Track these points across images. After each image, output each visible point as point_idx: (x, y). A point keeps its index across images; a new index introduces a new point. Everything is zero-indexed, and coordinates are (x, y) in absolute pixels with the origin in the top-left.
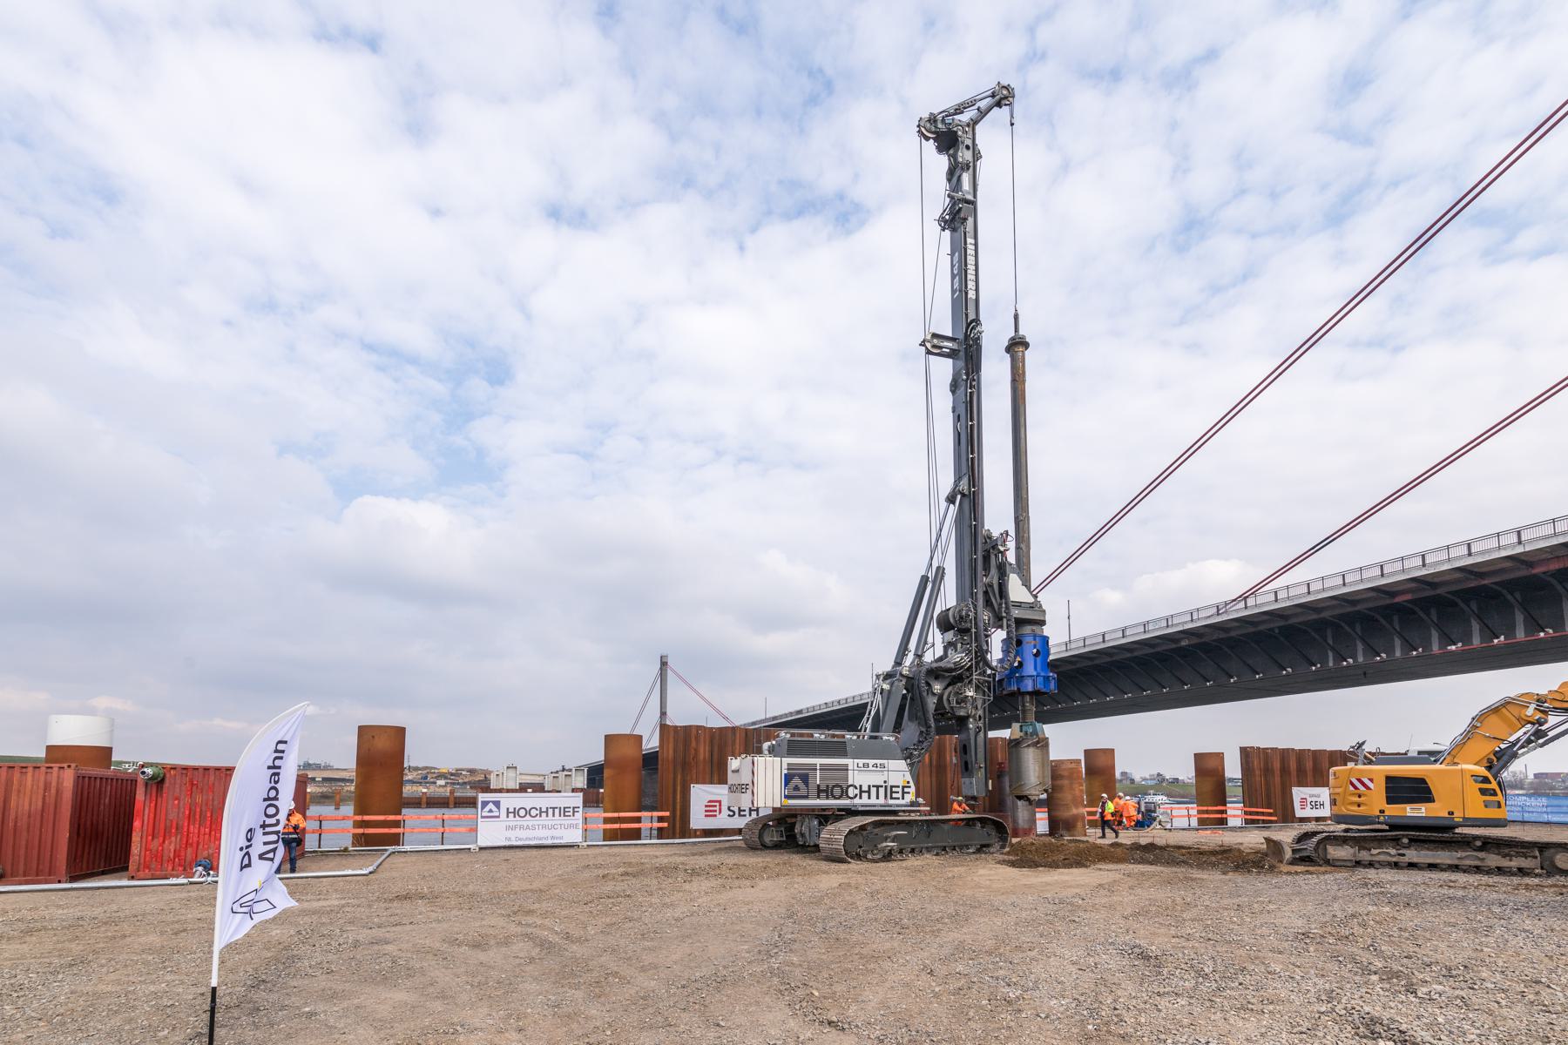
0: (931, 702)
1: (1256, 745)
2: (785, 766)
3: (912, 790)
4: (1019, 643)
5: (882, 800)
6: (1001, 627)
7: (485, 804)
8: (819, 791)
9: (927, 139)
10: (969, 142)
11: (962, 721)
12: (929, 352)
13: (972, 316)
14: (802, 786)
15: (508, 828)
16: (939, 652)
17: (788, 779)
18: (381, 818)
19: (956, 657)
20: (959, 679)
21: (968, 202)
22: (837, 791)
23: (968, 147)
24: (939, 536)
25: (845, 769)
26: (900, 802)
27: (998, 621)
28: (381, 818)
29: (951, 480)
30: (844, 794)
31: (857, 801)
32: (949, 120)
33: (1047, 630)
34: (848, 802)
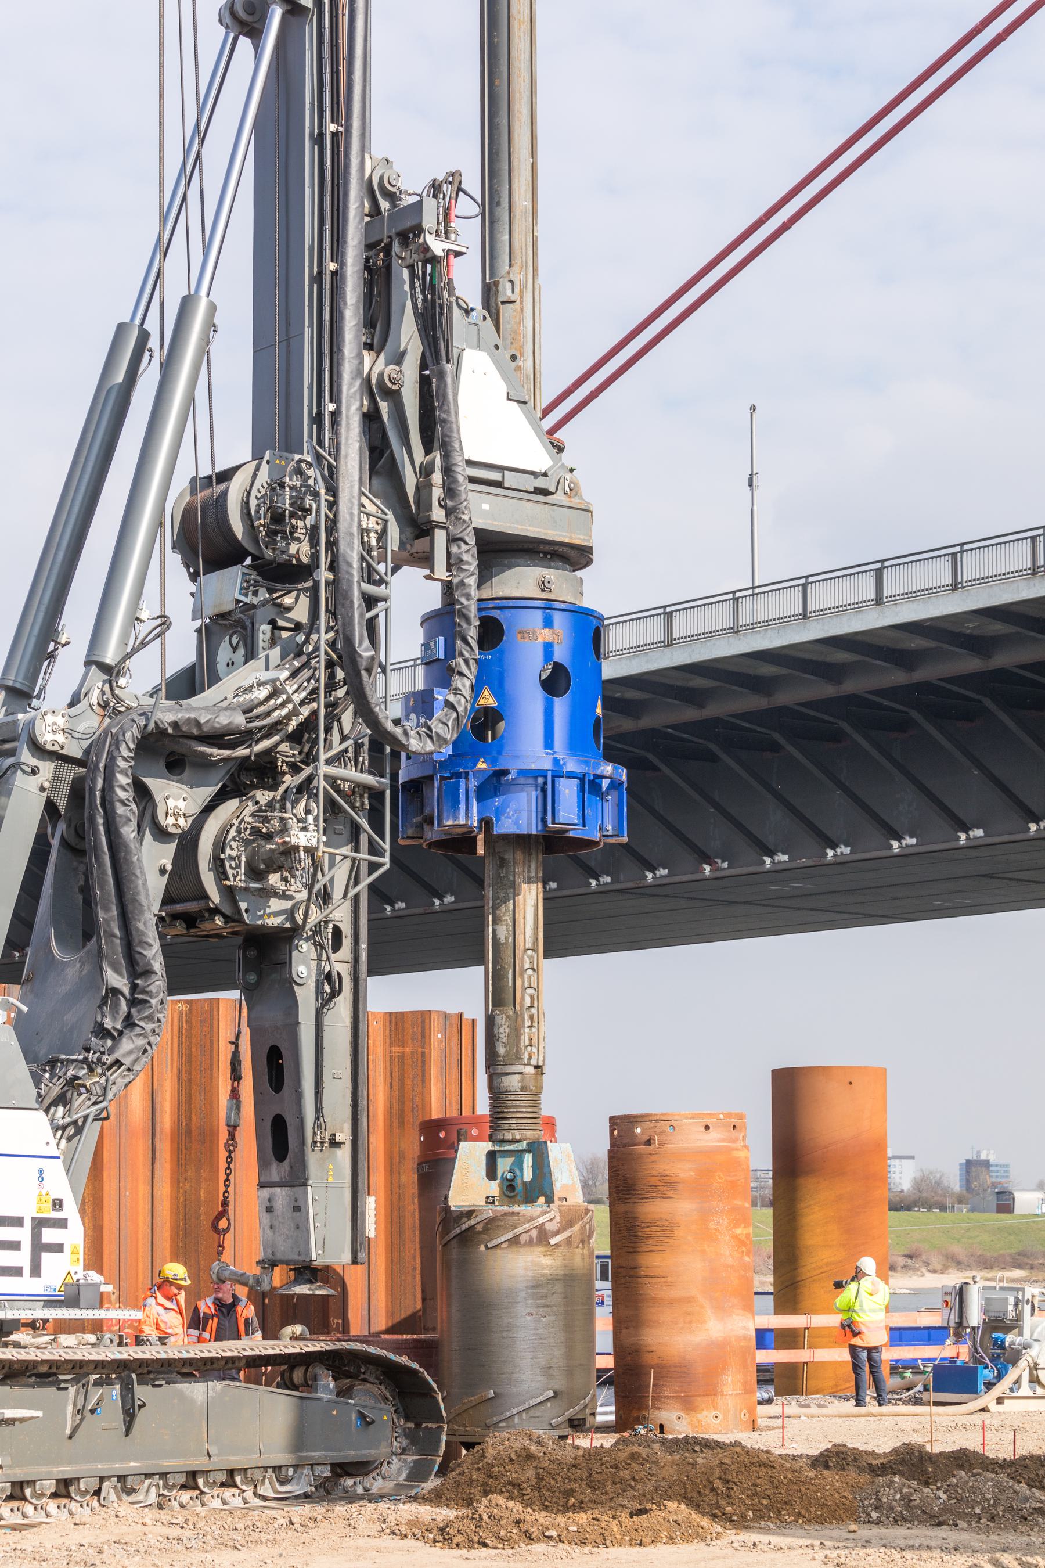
0: (152, 863)
3: (74, 1235)
4: (491, 633)
6: (426, 560)
16: (182, 650)
18: (306, 309)
19: (250, 686)
20: (264, 771)
24: (192, 168)
26: (25, 1284)
28: (306, 309)
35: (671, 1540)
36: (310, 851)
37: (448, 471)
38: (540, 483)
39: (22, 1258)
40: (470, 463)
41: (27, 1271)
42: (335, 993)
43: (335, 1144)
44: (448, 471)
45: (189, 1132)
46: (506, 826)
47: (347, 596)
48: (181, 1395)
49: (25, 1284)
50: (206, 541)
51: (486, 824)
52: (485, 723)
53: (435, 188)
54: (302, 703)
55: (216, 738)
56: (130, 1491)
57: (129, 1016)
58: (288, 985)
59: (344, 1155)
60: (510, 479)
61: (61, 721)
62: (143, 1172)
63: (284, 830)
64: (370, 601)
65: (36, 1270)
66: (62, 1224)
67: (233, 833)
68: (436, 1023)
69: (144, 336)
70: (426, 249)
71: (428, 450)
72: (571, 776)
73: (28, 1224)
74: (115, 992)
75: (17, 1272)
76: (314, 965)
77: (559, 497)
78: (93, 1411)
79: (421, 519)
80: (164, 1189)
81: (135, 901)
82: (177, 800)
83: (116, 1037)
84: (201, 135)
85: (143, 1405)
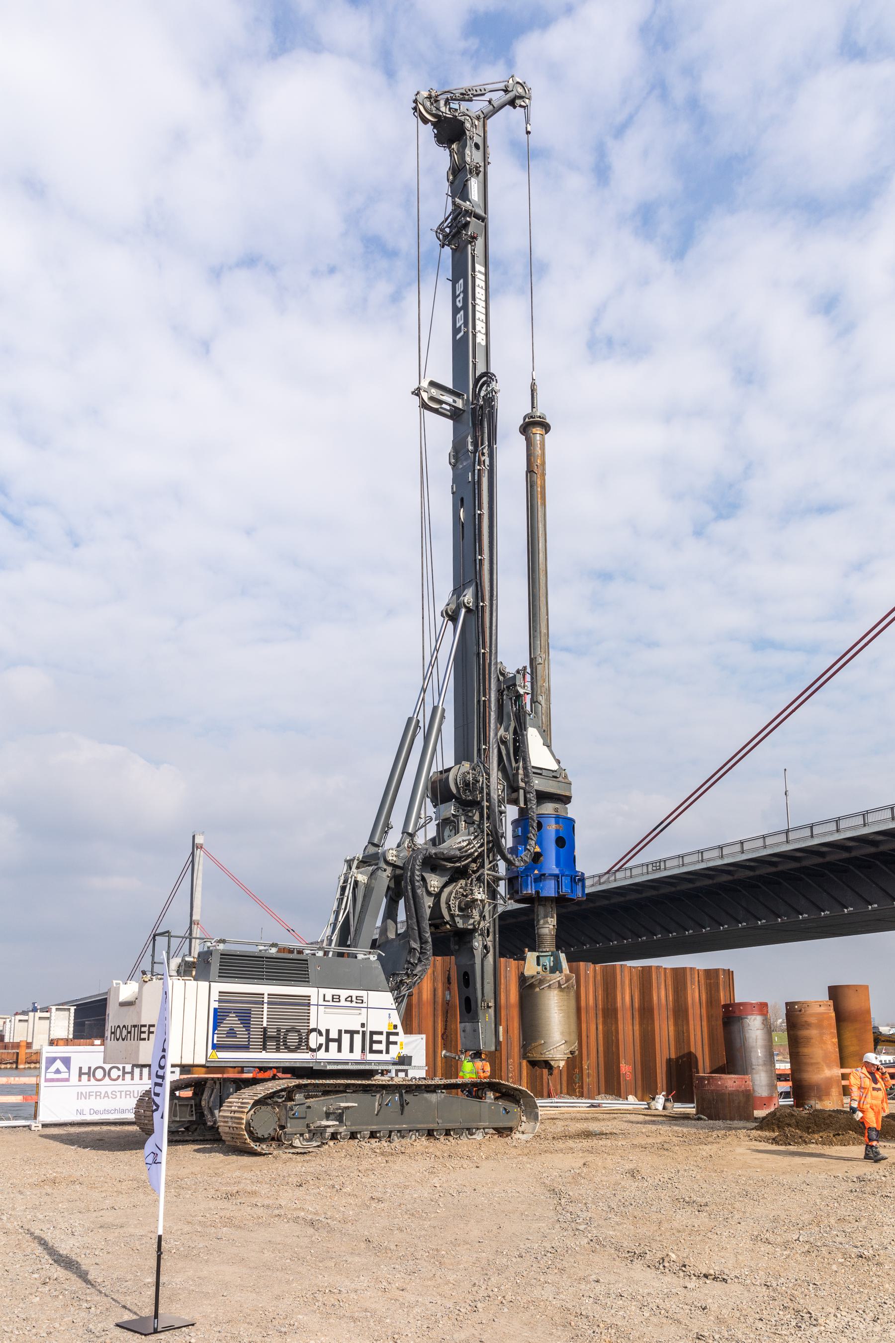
2: (215, 996)
5: (357, 1055)
7: (51, 1061)
8: (266, 1038)
9: (425, 121)
10: (478, 140)
11: (464, 937)
12: (424, 406)
13: (481, 369)
14: (240, 1029)
15: (80, 1095)
17: (219, 1017)
19: (461, 841)
21: (478, 217)
22: (293, 1039)
26: (383, 1057)
29: (450, 587)
30: (302, 1044)
31: (321, 1055)
32: (454, 105)
33: (572, 811)
34: (307, 1056)
35: (854, 1144)
36: (482, 901)
37: (525, 768)
38: (554, 774)
39: (383, 1047)
40: (533, 767)
41: (384, 1052)
42: (488, 952)
43: (489, 1007)
44: (525, 768)
45: (644, 1009)
46: (544, 894)
47: (494, 811)
48: (426, 1099)
49: (383, 1057)
50: (440, 791)
51: (538, 893)
52: (537, 857)
53: (518, 672)
54: (479, 847)
55: (450, 859)
56: (403, 1137)
57: (419, 958)
58: (472, 949)
59: (492, 1011)
60: (544, 773)
61: (395, 852)
62: (630, 1021)
63: (472, 894)
64: (501, 813)
65: (388, 1052)
66: (397, 1034)
67: (453, 895)
68: (721, 973)
69: (418, 721)
70: (518, 692)
71: (517, 761)
72: (567, 876)
73: (385, 1034)
74: (415, 949)
75: (380, 1052)
76: (481, 943)
77: (560, 779)
78: (387, 1105)
79: (515, 785)
80: (637, 1027)
81: (422, 916)
82: (435, 882)
83: (415, 966)
84: (437, 650)
85: (407, 1104)
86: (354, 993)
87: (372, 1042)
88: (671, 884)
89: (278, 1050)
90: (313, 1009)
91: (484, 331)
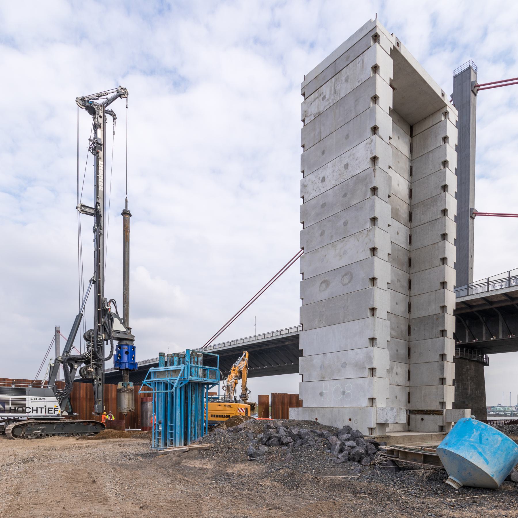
1: (277, 392)
21: (101, 145)
23: (101, 117)
25: (25, 400)
26: (53, 414)
27: (109, 337)
30: (24, 410)
31: (31, 414)
39: (53, 412)
86: (42, 397)
87: (49, 410)
88: (266, 345)
89: (15, 413)
90: (27, 402)
91: (102, 185)
